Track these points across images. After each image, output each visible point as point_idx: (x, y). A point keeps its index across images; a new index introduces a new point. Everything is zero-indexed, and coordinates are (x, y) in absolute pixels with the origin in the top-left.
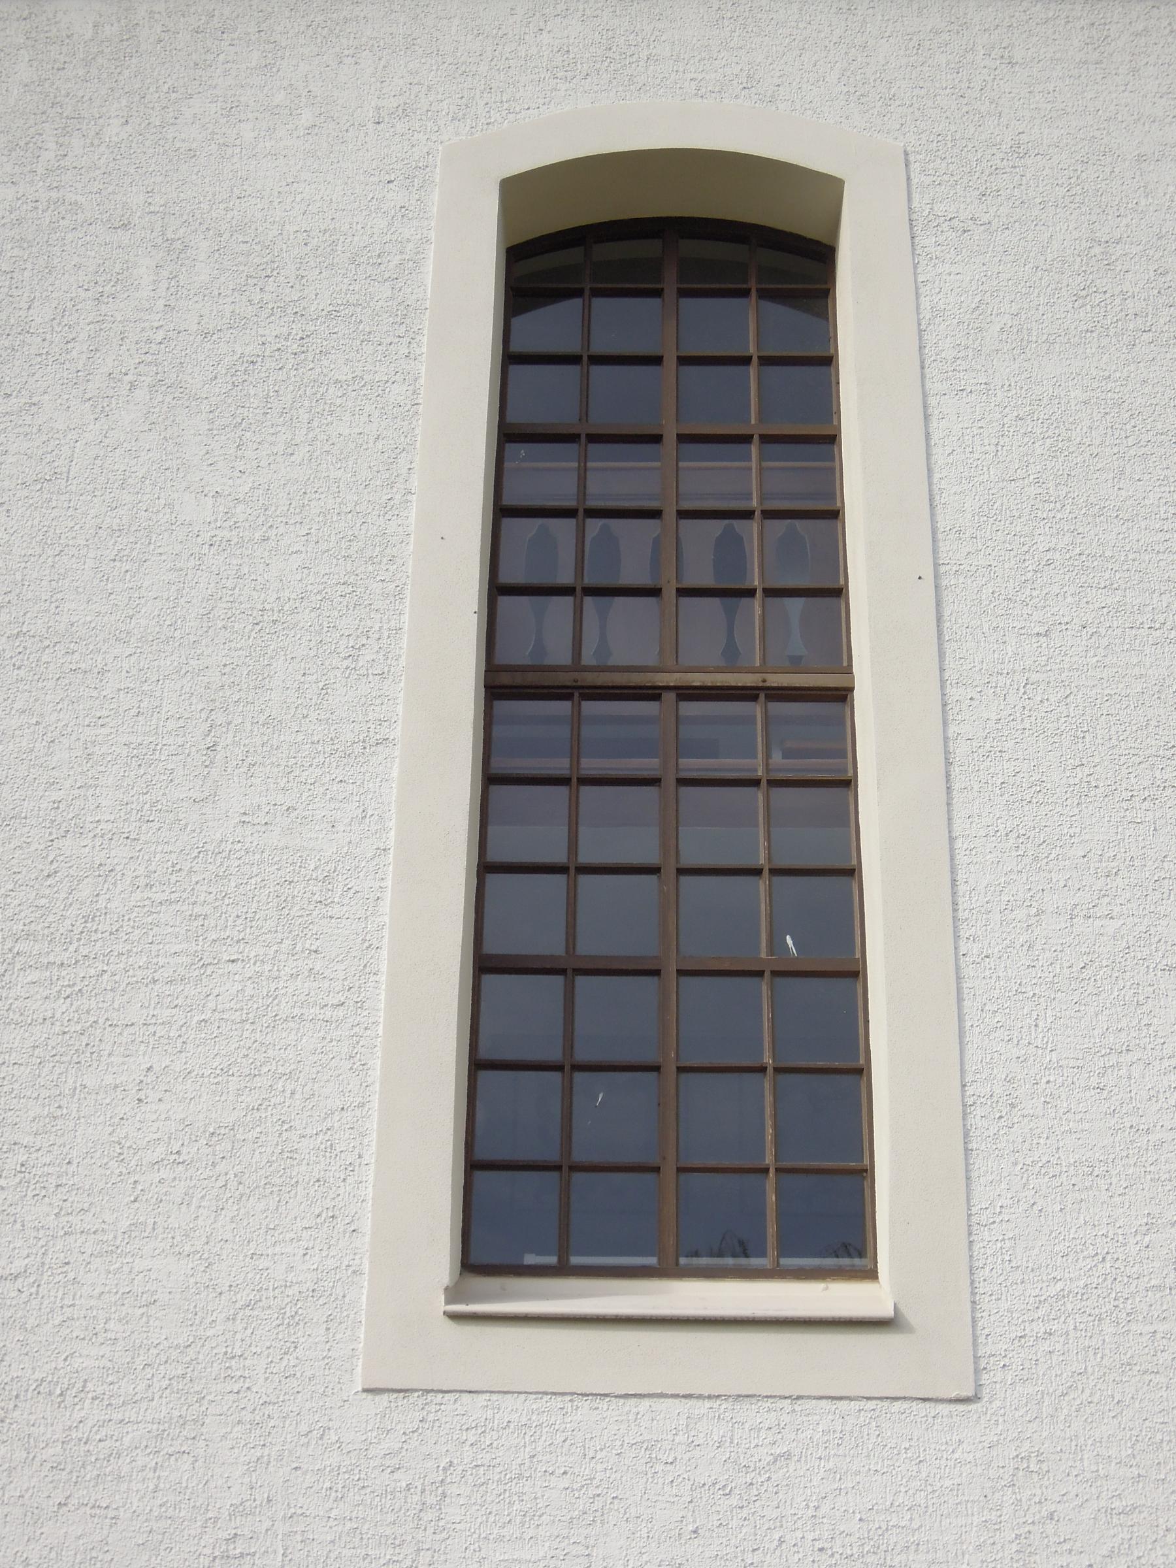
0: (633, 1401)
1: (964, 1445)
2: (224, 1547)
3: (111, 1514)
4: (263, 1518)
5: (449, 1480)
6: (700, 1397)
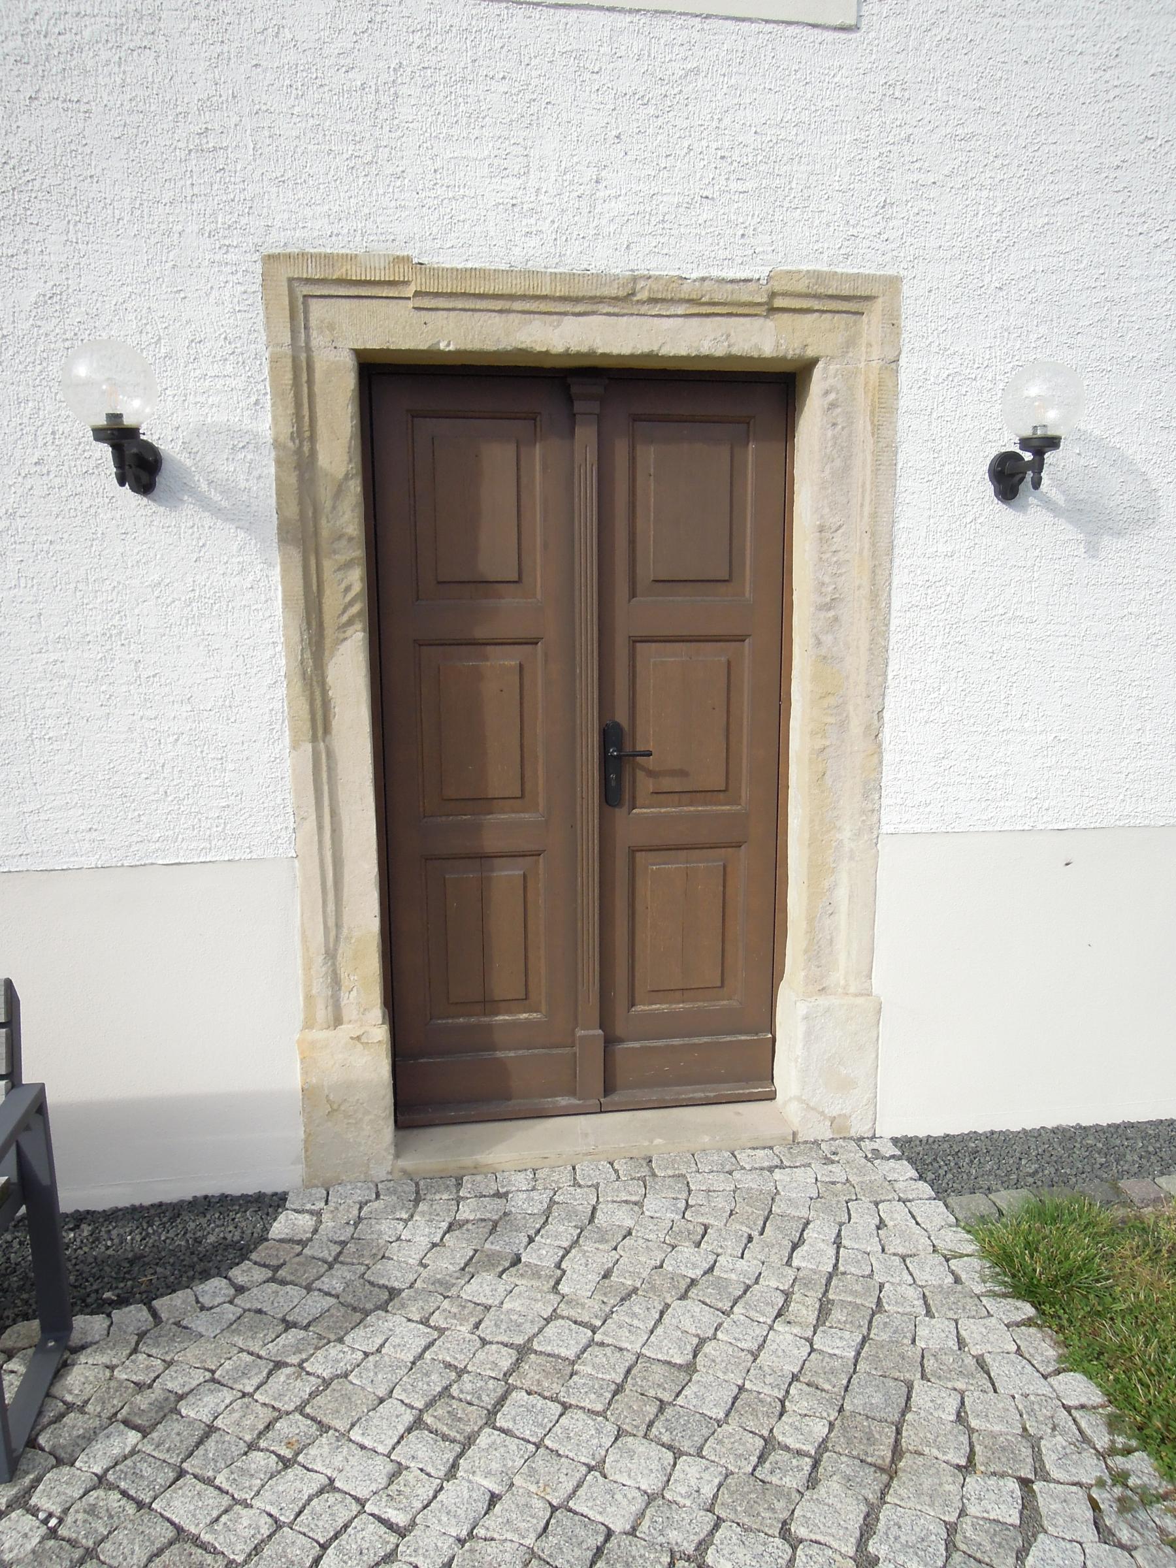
0: (563, 11)
1: (844, 71)
2: (197, 141)
3: (83, 108)
4: (231, 114)
5: (399, 81)
6: (622, 11)
